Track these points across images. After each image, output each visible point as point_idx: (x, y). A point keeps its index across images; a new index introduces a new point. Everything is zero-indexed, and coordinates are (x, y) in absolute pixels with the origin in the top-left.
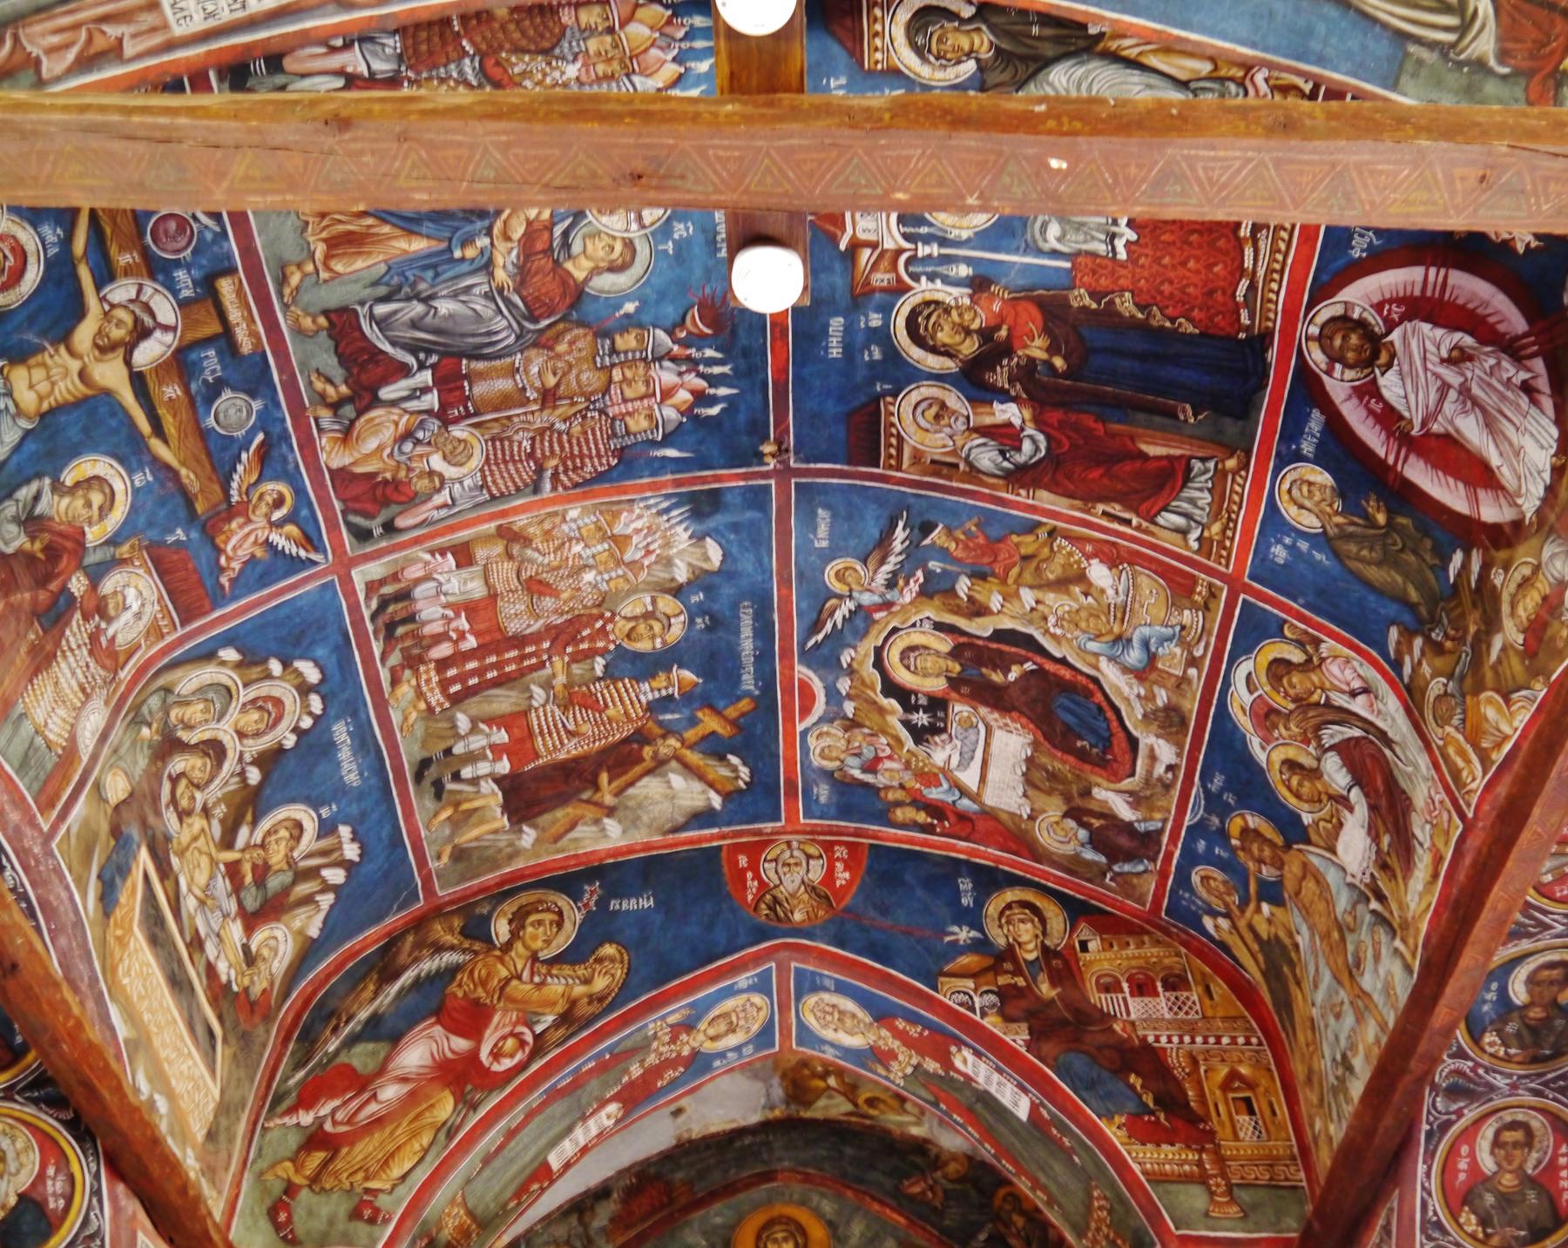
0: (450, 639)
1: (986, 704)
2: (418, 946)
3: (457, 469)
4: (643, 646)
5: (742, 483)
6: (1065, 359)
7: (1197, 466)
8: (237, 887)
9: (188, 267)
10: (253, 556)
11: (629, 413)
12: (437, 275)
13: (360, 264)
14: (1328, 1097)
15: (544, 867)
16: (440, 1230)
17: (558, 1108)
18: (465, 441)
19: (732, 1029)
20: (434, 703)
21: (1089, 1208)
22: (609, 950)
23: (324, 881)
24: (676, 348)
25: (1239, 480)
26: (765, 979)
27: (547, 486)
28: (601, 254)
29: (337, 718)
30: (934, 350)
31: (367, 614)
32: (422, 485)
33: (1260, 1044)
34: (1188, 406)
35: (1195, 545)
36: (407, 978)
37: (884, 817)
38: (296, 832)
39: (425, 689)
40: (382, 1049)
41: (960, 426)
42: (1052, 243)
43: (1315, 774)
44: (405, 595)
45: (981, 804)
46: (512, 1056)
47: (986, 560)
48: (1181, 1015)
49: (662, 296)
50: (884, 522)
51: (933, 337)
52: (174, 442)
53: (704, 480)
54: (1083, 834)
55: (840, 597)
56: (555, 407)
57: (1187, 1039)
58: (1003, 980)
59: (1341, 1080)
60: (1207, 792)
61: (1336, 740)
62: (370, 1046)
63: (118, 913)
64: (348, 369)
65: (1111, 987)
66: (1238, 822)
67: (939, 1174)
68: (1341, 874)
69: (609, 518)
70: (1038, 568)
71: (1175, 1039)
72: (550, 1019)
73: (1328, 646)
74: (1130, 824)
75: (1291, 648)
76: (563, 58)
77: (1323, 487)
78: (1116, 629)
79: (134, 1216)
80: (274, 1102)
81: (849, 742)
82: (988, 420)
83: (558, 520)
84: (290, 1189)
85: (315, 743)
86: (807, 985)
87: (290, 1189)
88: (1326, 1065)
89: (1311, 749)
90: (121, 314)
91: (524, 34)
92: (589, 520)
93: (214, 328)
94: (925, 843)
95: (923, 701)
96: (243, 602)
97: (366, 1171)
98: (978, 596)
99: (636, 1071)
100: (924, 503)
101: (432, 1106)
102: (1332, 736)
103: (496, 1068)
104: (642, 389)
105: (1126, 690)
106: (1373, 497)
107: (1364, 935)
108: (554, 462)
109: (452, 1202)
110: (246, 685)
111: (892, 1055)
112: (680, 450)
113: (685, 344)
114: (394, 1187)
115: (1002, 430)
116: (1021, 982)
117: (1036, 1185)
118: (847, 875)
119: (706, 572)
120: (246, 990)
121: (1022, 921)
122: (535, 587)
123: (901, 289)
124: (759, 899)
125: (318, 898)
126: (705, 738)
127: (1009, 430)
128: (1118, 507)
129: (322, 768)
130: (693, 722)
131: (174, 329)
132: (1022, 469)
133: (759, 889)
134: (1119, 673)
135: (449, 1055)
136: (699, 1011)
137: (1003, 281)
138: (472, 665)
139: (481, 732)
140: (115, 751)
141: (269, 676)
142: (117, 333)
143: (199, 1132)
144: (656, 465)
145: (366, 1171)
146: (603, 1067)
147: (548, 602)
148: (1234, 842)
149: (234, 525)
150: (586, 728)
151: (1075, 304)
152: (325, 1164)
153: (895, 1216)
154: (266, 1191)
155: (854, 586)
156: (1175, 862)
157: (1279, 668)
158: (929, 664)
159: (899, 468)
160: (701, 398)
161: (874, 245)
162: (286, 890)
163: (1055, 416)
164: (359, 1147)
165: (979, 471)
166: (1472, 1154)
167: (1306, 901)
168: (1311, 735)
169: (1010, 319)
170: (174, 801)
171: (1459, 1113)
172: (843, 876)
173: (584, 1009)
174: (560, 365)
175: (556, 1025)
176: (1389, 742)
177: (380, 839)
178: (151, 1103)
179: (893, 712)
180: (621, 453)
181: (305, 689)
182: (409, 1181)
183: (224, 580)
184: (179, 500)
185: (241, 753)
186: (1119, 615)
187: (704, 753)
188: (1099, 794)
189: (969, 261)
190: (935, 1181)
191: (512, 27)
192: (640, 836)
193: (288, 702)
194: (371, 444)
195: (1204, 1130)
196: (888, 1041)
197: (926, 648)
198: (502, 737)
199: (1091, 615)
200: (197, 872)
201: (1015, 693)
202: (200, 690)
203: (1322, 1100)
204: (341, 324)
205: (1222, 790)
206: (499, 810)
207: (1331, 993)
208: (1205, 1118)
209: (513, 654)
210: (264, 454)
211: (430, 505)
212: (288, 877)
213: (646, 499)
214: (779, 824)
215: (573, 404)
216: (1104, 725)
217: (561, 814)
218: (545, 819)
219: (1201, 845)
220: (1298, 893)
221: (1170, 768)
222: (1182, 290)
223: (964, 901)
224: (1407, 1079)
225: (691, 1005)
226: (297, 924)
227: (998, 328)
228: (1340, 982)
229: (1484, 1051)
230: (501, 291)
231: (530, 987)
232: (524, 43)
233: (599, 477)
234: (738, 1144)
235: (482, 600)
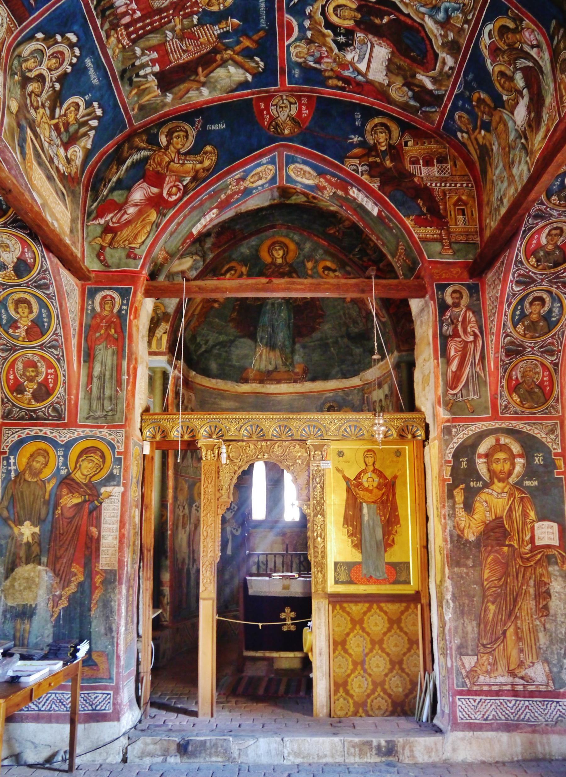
0: (129, 14)
1: (372, 34)
4: (215, 8)
8: (59, 134)
14: (493, 212)
15: (177, 110)
16: (158, 259)
17: (195, 213)
21: (397, 249)
22: (209, 148)
23: (90, 125)
31: (92, 7)
33: (472, 187)
36: (129, 162)
37: (323, 83)
38: (77, 108)
39: (121, 38)
40: (125, 193)
43: (511, 79)
45: (367, 78)
46: (176, 195)
48: (442, 174)
54: (410, 93)
57: (443, 184)
58: (371, 160)
60: (466, 81)
61: (523, 65)
63: (27, 157)
65: (415, 162)
66: (477, 95)
67: (341, 225)
71: (438, 185)
73: (526, 22)
74: (431, 91)
75: (510, 21)
80: (88, 215)
81: (308, 50)
84: (102, 248)
85: (79, 69)
86: (291, 161)
87: (102, 248)
88: (494, 199)
89: (511, 68)
95: (343, 31)
99: (223, 197)
101: (148, 215)
102: (521, 64)
103: (170, 199)
105: (435, 31)
107: (517, 151)
109: (161, 250)
110: (48, 48)
114: (140, 246)
116: (378, 160)
118: (307, 112)
120: (70, 174)
121: (381, 132)
124: (270, 124)
130: (238, 42)
133: (270, 119)
134: (433, 23)
135: (151, 195)
136: (247, 173)
138: (140, 25)
139: (146, 54)
140: (10, 90)
141: (57, 42)
146: (211, 197)
148: (474, 103)
150: (191, 48)
152: (113, 238)
153: (324, 242)
154: (93, 249)
157: (503, 30)
162: (77, 131)
164: (124, 232)
166: (539, 238)
168: (512, 62)
170: (32, 105)
171: (537, 224)
172: (305, 112)
173: (202, 175)
175: (191, 181)
176: (542, 72)
177: (109, 106)
178: (53, 223)
179: (329, 36)
181: (72, 46)
185: (51, 78)
190: (340, 229)
192: (217, 94)
193: (66, 52)
195: (444, 222)
198: (155, 55)
200: (45, 132)
202: (32, 53)
206: (156, 87)
207: (501, 173)
208: (446, 217)
212: (76, 126)
218: (176, 90)
219: (460, 103)
220: (496, 128)
221: (451, 68)
223: (357, 123)
224: (517, 215)
225: (244, 171)
228: (505, 169)
229: (551, 202)
231: (178, 165)
234: (260, 214)
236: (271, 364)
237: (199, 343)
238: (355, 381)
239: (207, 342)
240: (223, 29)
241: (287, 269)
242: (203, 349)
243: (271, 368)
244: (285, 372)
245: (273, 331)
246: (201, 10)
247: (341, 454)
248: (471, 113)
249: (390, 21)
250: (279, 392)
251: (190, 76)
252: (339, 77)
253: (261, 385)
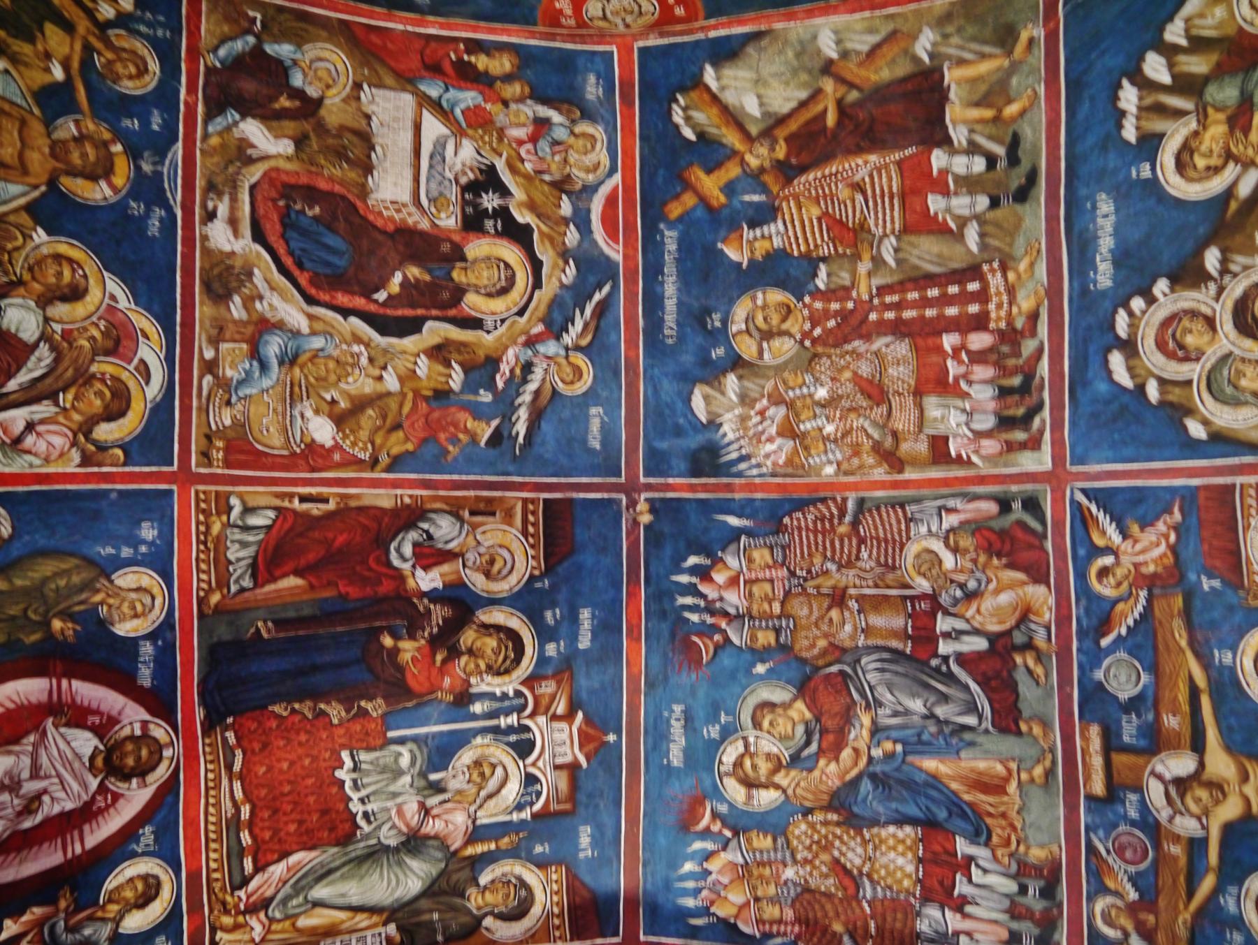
0: (968, 352)
1: (422, 234)
3: (931, 545)
4: (776, 296)
5: (671, 481)
6: (382, 647)
7: (247, 582)
9: (1125, 816)
10: (1142, 529)
11: (769, 567)
12: (919, 735)
13: (982, 765)
18: (919, 573)
20: (999, 275)
23: (1171, 66)
24: (724, 625)
25: (204, 586)
27: (850, 505)
28: (780, 721)
29: (1103, 294)
30: (498, 628)
31: (1046, 412)
32: (966, 542)
34: (265, 635)
35: (234, 501)
37: (524, 56)
38: (1186, 157)
39: (1005, 298)
41: (470, 557)
42: (405, 751)
44: (1005, 423)
47: (436, 415)
49: (733, 675)
50: (537, 439)
51: (500, 640)
52: (1183, 675)
53: (705, 488)
54: (297, 80)
55: (578, 348)
56: (834, 588)
64: (1011, 676)
66: (119, 180)
69: (796, 460)
70: (384, 417)
73: (72, 465)
74: (244, 116)
75: (110, 438)
76: (795, 884)
77: (123, 619)
78: (297, 371)
81: (565, 161)
82: (446, 568)
83: (845, 466)
85: (1136, 276)
89: (58, 328)
90: (1194, 808)
91: (823, 907)
92: (815, 460)
93: (1119, 759)
95: (489, 224)
96: (1165, 482)
98: (441, 368)
100: (500, 468)
104: (755, 589)
105: (276, 301)
106: (71, 639)
108: (842, 529)
110: (1189, 382)
112: (725, 523)
113: (715, 628)
115: (431, 561)
119: (708, 383)
122: (875, 392)
123: (529, 681)
125: (1183, 42)
126: (719, 165)
127: (425, 562)
128: (315, 512)
129: (1135, 235)
130: (730, 189)
131: (1153, 773)
132: (411, 525)
134: (288, 319)
137: (443, 706)
138: (952, 311)
141: (1162, 382)
142: (1203, 794)
144: (748, 511)
147: (865, 369)
149: (1152, 568)
150: (844, 192)
151: (380, 701)
155: (563, 362)
158: (485, 274)
159: (525, 501)
160: (704, 574)
161: (555, 718)
162: (1219, 72)
163: (386, 588)
165: (450, 513)
168: (61, 345)
169: (434, 672)
174: (825, 628)
177: (1092, 99)
179: (521, 205)
180: (779, 529)
181: (1129, 347)
183: (1177, 516)
184: (1196, 619)
186: (296, 389)
187: (723, 145)
188: (285, 147)
189: (475, 717)
191: (831, 914)
192: (794, 28)
194: (1005, 598)
197: (489, 295)
198: (935, 203)
199: (325, 379)
201: (393, 257)
204: (1008, 719)
205: (147, 215)
206: (952, 95)
209: (909, 314)
210: (1105, 625)
211: (962, 517)
213: (760, 475)
214: (641, 44)
215: (818, 587)
216: (293, 244)
217: (883, 73)
219: (156, 123)
220: (23, 123)
221: (211, 216)
222: (289, 741)
227: (444, 662)
230: (868, 706)
232: (823, 900)
233: (801, 505)
235: (929, 393)
240: (763, 236)
246: (807, 299)
248: (112, 107)
249: (382, 284)
251: (859, 104)
252: (483, 81)
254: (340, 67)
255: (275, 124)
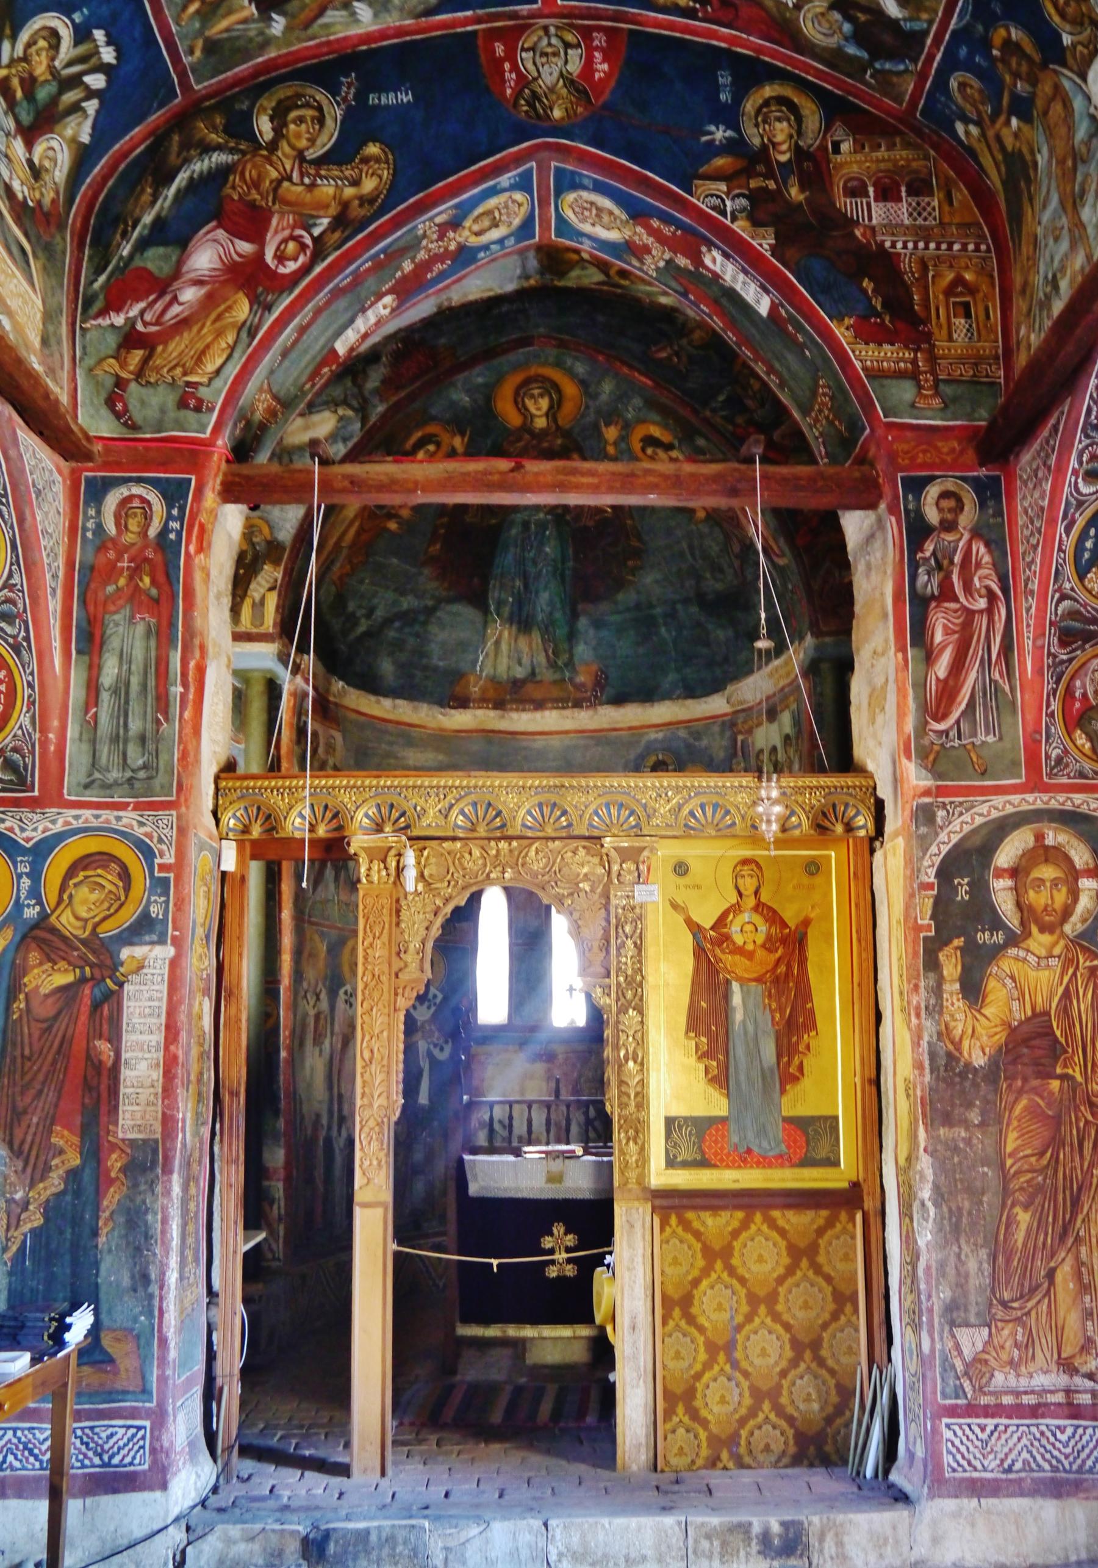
2: (186, 146)
14: (1036, 310)
15: (296, 57)
16: (253, 413)
17: (342, 303)
19: (495, 225)
21: (814, 393)
22: (373, 149)
23: (87, 87)
26: (527, 176)
33: (988, 250)
36: (181, 179)
38: (54, 41)
40: (174, 253)
46: (296, 259)
48: (920, 221)
54: (847, 27)
57: (921, 245)
58: (753, 184)
59: (1048, 297)
62: (161, 250)
65: (856, 191)
67: (684, 342)
68: (1086, 102)
71: (910, 245)
72: (325, 221)
74: (896, 21)
79: (10, 419)
80: (86, 305)
84: (120, 383)
86: (567, 183)
87: (120, 383)
88: (1038, 280)
94: (686, 29)
97: (184, 366)
99: (408, 266)
103: (282, 270)
109: (261, 390)
111: (647, 250)
116: (772, 185)
117: (771, 370)
118: (605, 67)
120: (39, 203)
121: (779, 119)
124: (518, 94)
125: (84, 104)
133: (517, 82)
143: (36, 341)
145: (184, 366)
146: (378, 266)
148: (995, 52)
152: (145, 361)
154: (98, 384)
156: (935, 65)
162: (54, 100)
164: (172, 346)
167: (1052, 122)
177: (134, 40)
182: (223, 375)
192: (392, 20)
195: (923, 332)
196: (642, 236)
203: (1030, 310)
212: (53, 88)
214: (535, 6)
219: (963, 51)
220: (1046, 113)
223: (723, 97)
225: (456, 206)
226: (69, 132)
231: (300, 188)
234: (495, 312)
236: (520, 664)
237: (353, 614)
238: (716, 705)
239: (371, 611)
241: (559, 441)
242: (362, 628)
243: (520, 673)
244: (555, 682)
245: (526, 586)
247: (681, 869)
250: (539, 729)
253: (499, 712)
254: (809, 24)
255: (873, 6)
